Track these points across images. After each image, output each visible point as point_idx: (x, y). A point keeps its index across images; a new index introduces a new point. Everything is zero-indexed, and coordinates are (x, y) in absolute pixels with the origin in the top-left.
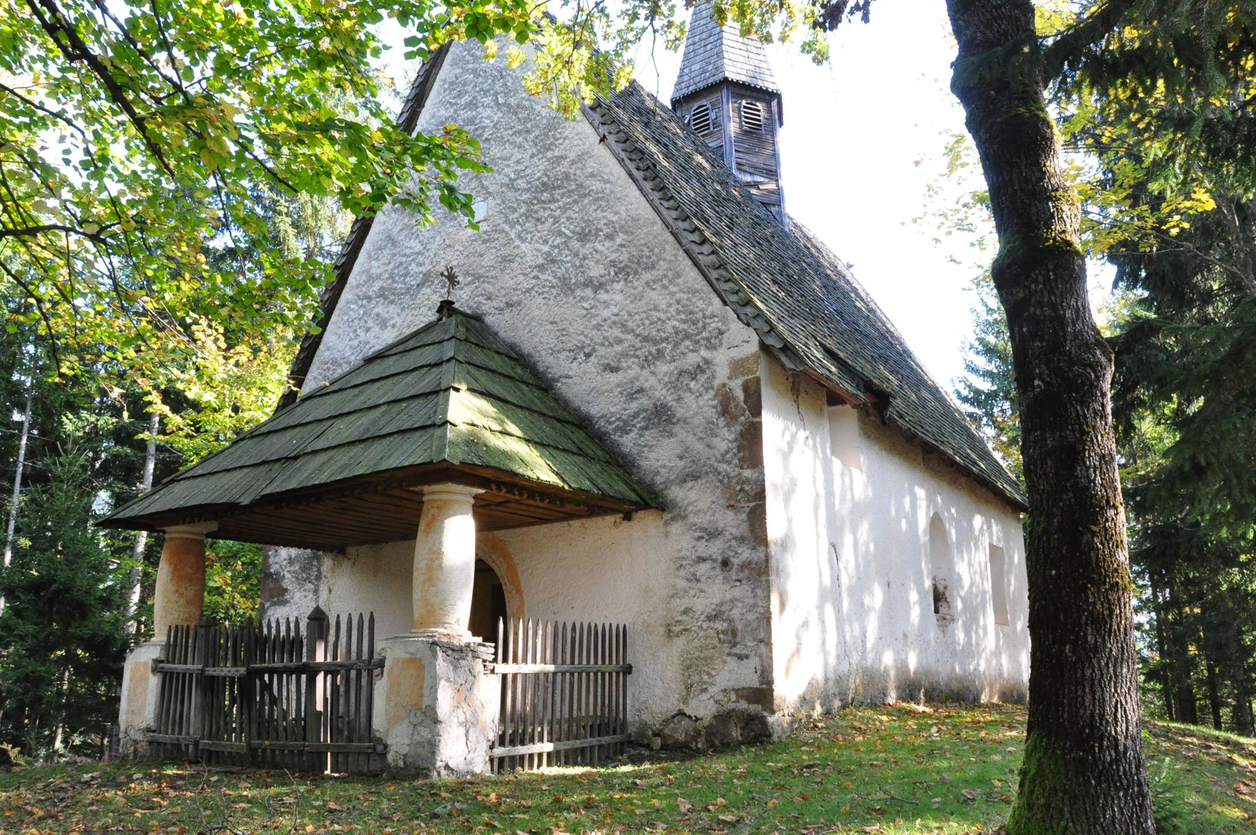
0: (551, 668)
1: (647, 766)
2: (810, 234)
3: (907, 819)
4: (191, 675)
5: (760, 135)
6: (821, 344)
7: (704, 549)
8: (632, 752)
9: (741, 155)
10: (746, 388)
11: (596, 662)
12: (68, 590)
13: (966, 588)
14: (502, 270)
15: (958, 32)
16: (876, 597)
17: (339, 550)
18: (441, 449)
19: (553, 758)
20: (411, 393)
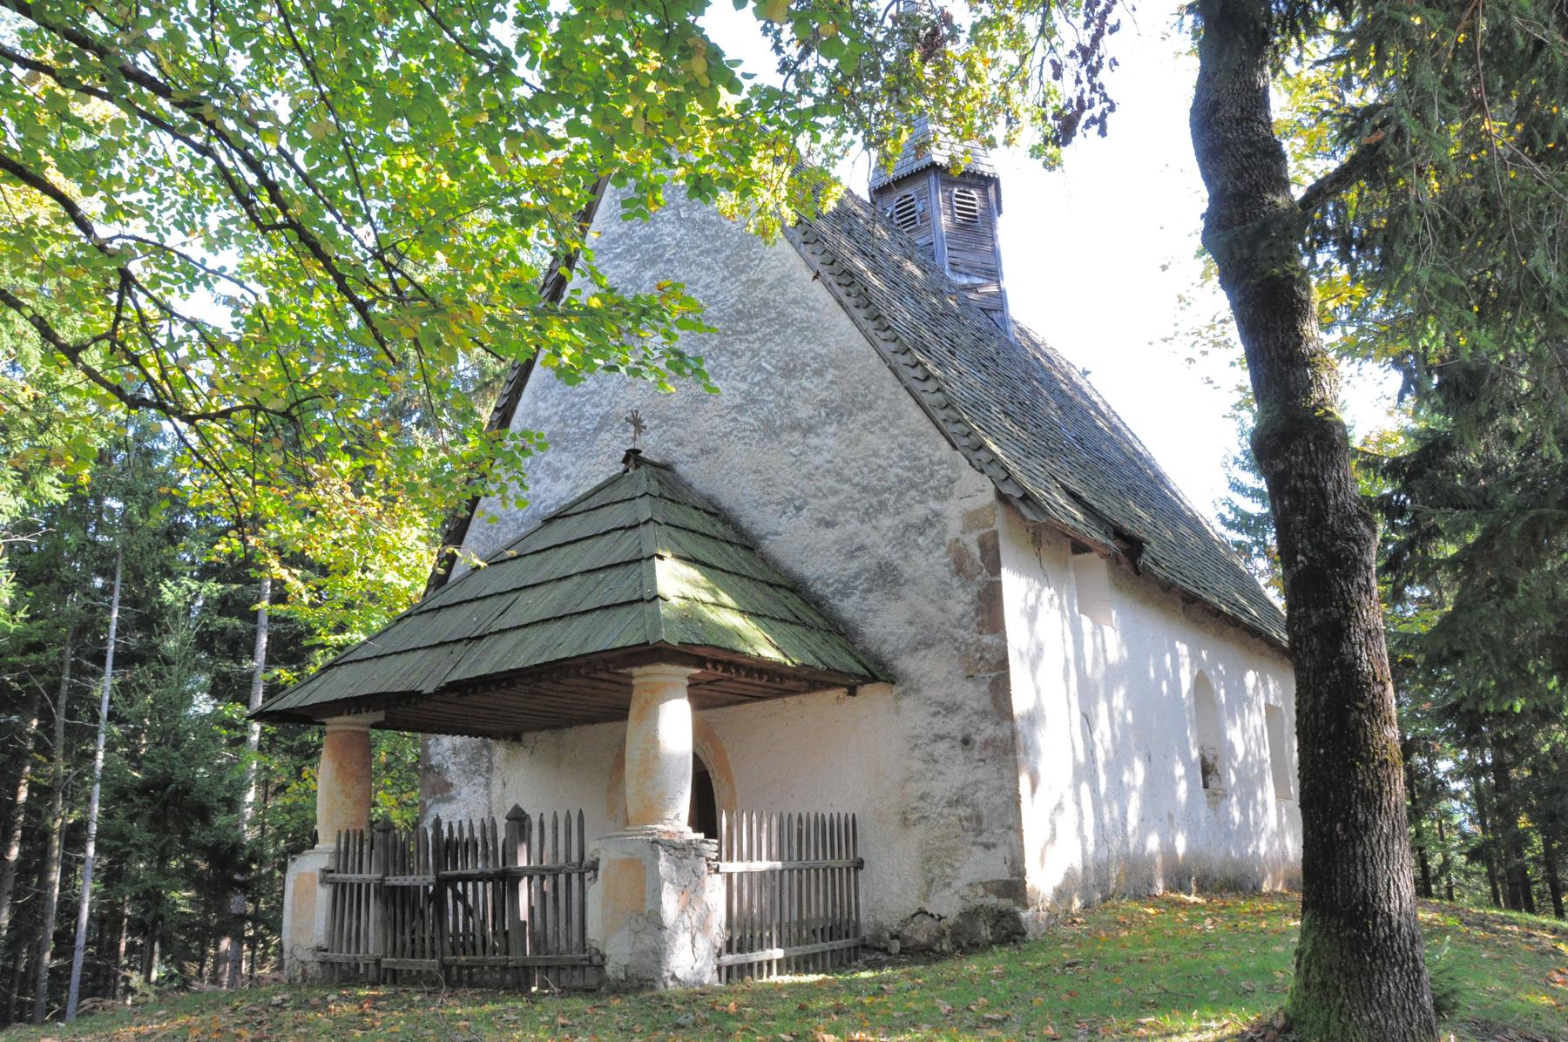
0: (779, 865)
1: (888, 971)
2: (1038, 340)
3: (1183, 1010)
4: (368, 885)
5: (977, 229)
6: (1063, 486)
7: (940, 725)
8: (868, 957)
9: (954, 253)
10: (982, 544)
11: (825, 857)
12: (187, 791)
13: (1240, 758)
14: (694, 412)
15: (1208, 179)
16: (1137, 774)
17: (514, 737)
18: (657, 631)
19: (785, 966)
20: (608, 562)
